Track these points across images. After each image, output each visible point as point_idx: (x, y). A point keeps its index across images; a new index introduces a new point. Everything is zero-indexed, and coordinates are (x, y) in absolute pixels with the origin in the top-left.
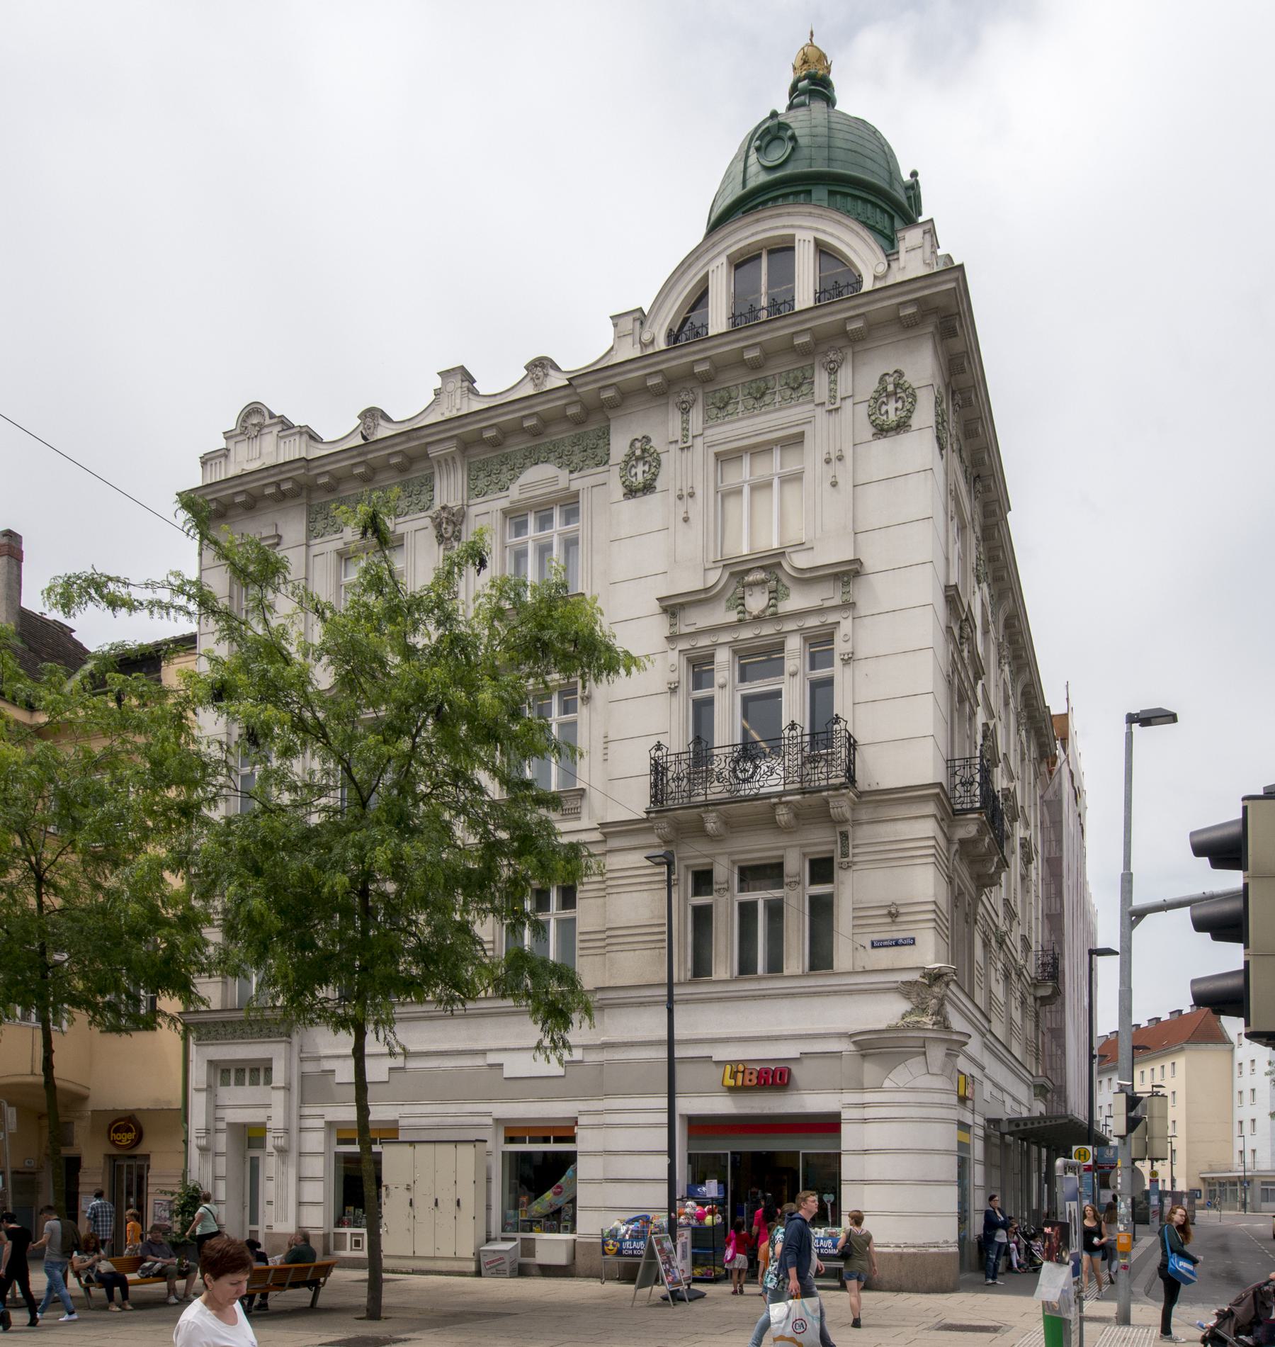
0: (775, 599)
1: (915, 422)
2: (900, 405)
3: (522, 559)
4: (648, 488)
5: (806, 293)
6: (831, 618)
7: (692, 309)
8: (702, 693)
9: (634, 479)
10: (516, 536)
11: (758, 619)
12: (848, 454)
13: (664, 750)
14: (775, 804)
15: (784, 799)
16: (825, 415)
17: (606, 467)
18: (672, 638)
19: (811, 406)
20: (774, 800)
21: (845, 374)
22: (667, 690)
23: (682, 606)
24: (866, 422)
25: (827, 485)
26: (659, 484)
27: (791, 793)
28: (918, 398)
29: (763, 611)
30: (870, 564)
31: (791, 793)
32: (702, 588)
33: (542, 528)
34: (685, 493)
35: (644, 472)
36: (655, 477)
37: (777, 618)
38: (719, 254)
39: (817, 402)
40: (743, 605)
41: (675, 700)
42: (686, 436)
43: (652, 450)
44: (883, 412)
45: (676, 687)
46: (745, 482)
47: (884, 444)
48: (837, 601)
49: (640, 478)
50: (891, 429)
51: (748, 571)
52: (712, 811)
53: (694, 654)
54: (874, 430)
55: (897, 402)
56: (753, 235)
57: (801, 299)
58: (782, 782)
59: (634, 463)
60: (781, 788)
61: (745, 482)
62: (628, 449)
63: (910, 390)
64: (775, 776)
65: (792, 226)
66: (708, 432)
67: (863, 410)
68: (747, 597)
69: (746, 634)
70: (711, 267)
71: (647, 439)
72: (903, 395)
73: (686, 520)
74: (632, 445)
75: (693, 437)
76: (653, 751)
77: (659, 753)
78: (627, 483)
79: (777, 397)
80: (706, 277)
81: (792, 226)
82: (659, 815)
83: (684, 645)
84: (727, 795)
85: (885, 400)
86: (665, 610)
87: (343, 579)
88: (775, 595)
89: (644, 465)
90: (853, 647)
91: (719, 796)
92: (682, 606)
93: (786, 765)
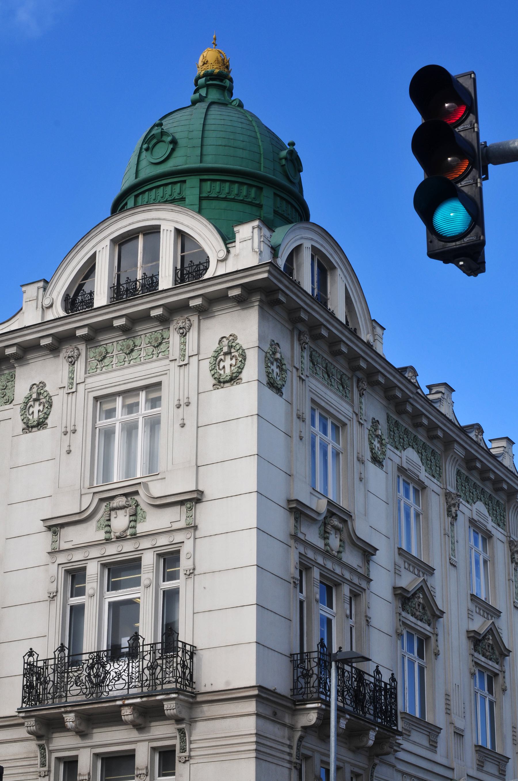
0: (135, 521)
1: (244, 375)
2: (233, 362)
3: (134, 431)
4: (41, 424)
5: (167, 270)
6: (178, 537)
7: (86, 277)
8: (75, 601)
9: (222, 372)
10: (152, 408)
11: (121, 538)
12: (193, 400)
13: (35, 656)
14: (121, 706)
15: (127, 702)
16: (177, 369)
17: (11, 406)
18: (54, 552)
19: (167, 362)
20: (119, 703)
21: (192, 336)
22: (47, 598)
23: (62, 526)
24: (209, 374)
25: (177, 426)
26: (49, 421)
27: (134, 697)
28: (247, 356)
29: (125, 531)
30: (209, 494)
31: (134, 697)
32: (79, 511)
33: (130, 412)
34: (68, 430)
35: (39, 411)
36: (240, 370)
37: (134, 536)
38: (104, 238)
39: (171, 358)
40: (110, 526)
41: (53, 605)
42: (72, 384)
43: (238, 347)
44: (221, 367)
45: (54, 596)
46: (117, 420)
47: (221, 392)
48: (182, 524)
49: (228, 371)
50: (227, 382)
51: (113, 498)
52: (70, 712)
53: (69, 567)
54: (214, 382)
55: (231, 359)
56: (130, 224)
57: (164, 275)
58: (126, 687)
59: (222, 357)
60: (125, 692)
61: (117, 420)
62: (29, 392)
63: (240, 351)
64: (121, 681)
65: (159, 219)
66: (88, 380)
67: (206, 365)
68: (112, 519)
69: (111, 549)
70: (98, 249)
71: (43, 384)
72: (236, 354)
73: (69, 452)
74: (31, 389)
75: (189, 357)
76: (26, 657)
77: (31, 659)
78: (216, 376)
79: (142, 353)
80: (94, 256)
81: (159, 219)
82: (28, 714)
83: (62, 558)
84: (84, 697)
85: (222, 357)
86: (49, 528)
87: (98, 422)
88: (134, 517)
89: (40, 405)
90: (194, 564)
91: (79, 698)
92: (62, 526)
93: (130, 671)
